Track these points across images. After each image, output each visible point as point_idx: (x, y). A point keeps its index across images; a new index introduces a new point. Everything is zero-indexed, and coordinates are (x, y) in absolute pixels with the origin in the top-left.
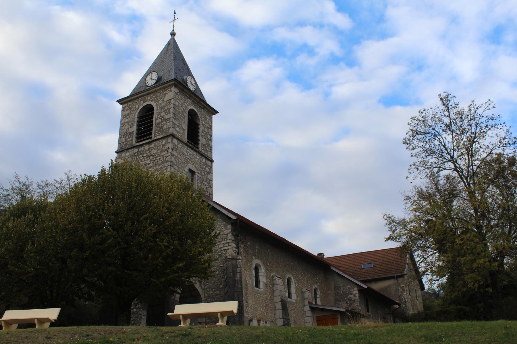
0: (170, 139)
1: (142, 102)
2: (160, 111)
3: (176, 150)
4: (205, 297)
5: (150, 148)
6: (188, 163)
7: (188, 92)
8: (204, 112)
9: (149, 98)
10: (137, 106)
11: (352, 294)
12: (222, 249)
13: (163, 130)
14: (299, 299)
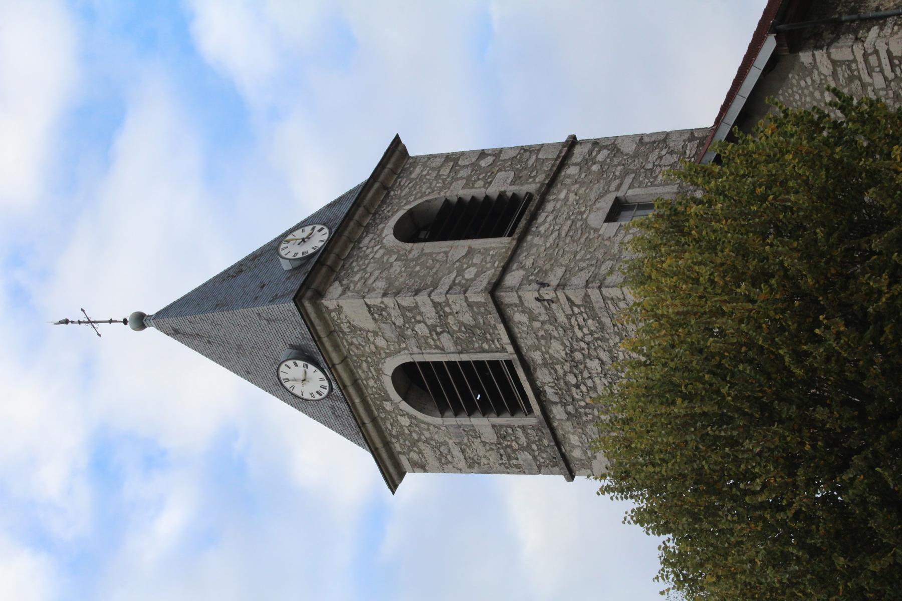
0: (508, 298)
1: (388, 406)
3: (546, 273)
5: (545, 365)
6: (586, 227)
7: (337, 250)
8: (401, 187)
9: (371, 383)
10: (405, 421)
12: (891, 76)
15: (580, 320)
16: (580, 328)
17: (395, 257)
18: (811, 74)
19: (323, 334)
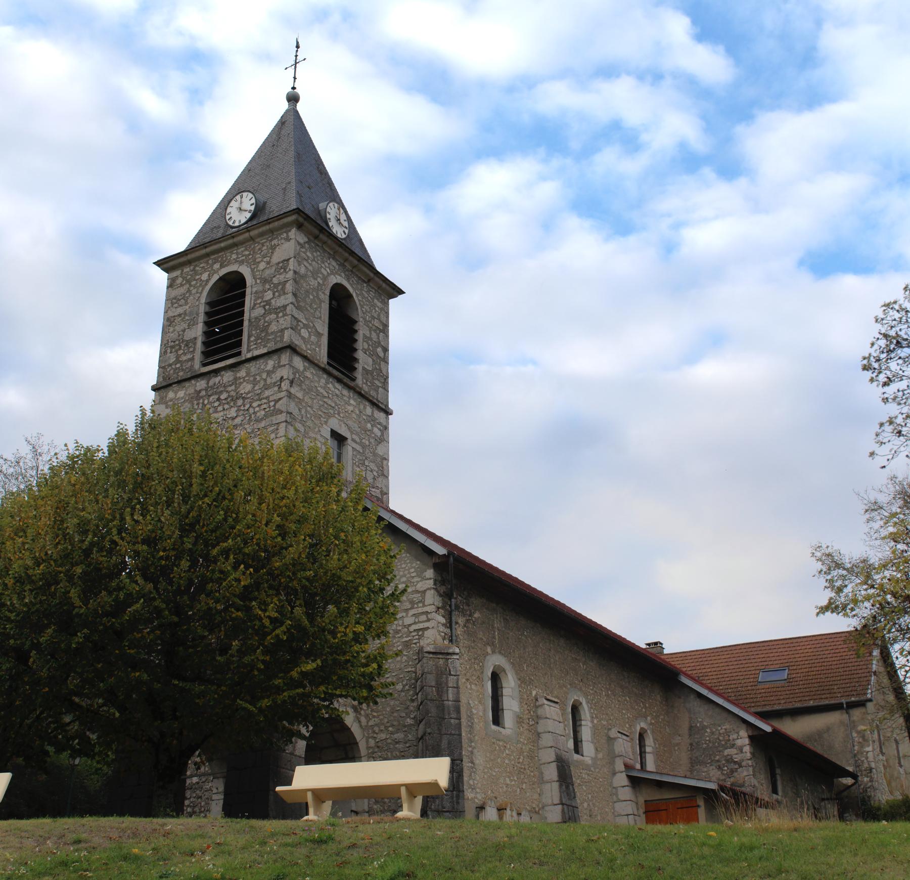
0: (285, 358)
1: (217, 266)
2: (261, 288)
3: (300, 385)
4: (368, 748)
5: (236, 379)
6: (329, 416)
7: (329, 242)
8: (369, 291)
9: (234, 256)
11: (733, 746)
12: (412, 628)
16: (259, 406)
17: (321, 282)
18: (418, 576)
19: (271, 226)
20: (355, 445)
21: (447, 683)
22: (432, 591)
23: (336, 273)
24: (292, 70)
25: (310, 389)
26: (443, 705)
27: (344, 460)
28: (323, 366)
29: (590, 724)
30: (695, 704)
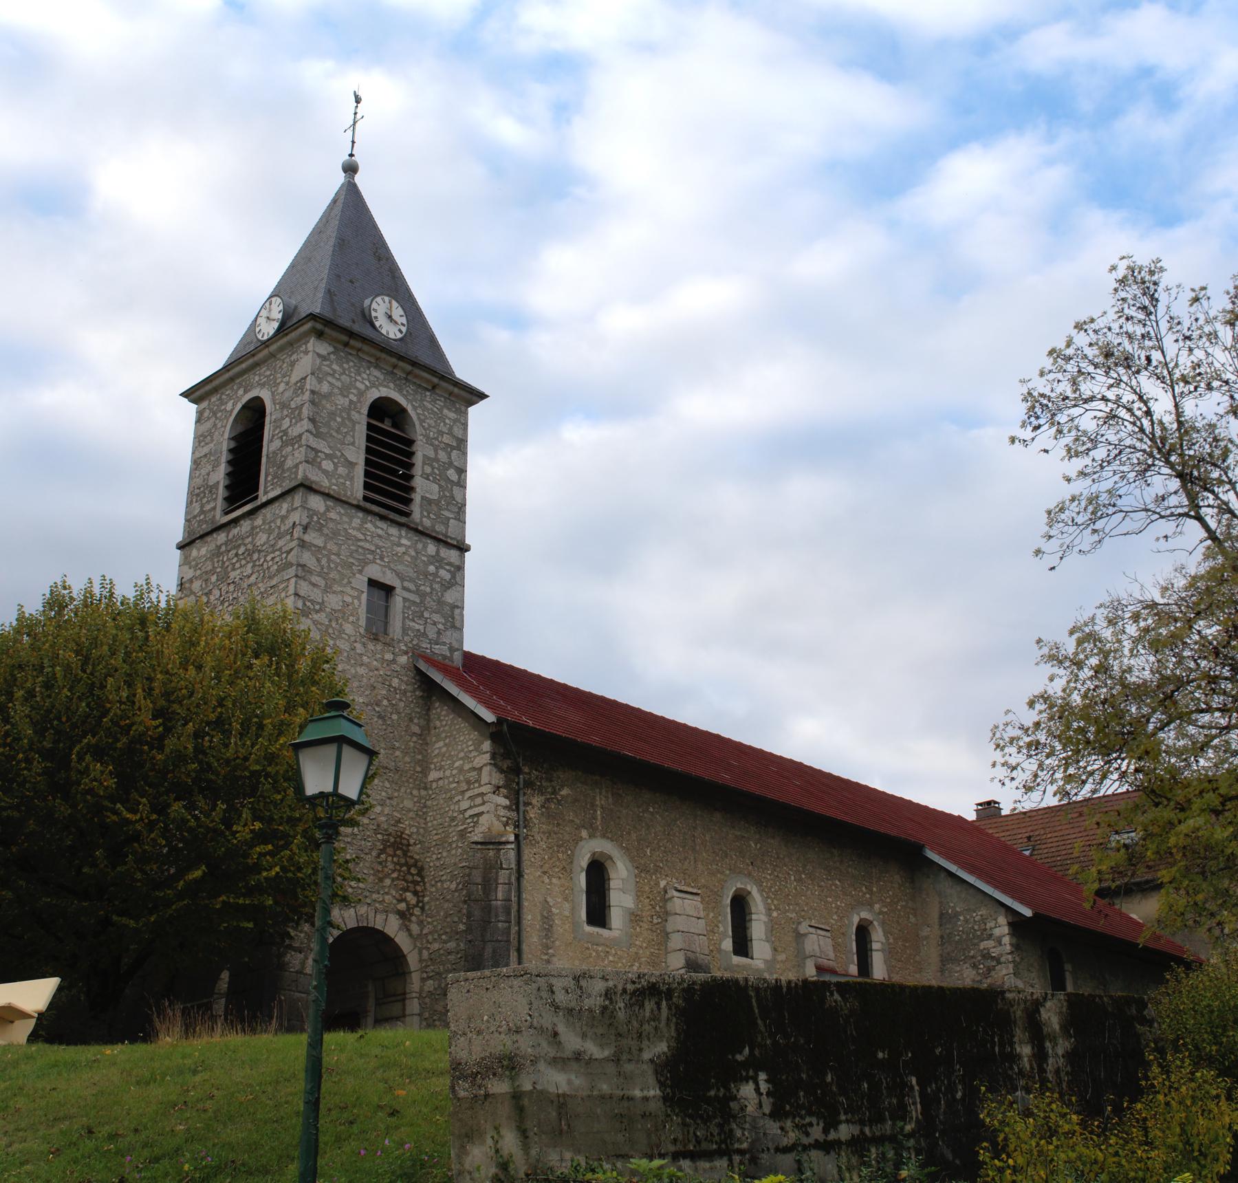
0: (298, 498)
1: (241, 392)
2: (279, 416)
3: (320, 530)
4: (421, 961)
5: (253, 528)
6: (365, 563)
7: (366, 348)
8: (434, 401)
9: (257, 378)
10: (229, 406)
11: (990, 936)
12: (467, 814)
13: (284, 471)
14: (782, 957)
15: (277, 559)
16: (273, 559)
17: (355, 399)
18: (476, 750)
20: (406, 594)
21: (496, 879)
22: (488, 768)
23: (381, 385)
24: (350, 132)
25: (336, 533)
26: (490, 905)
27: (391, 614)
28: (355, 502)
29: (764, 918)
30: (945, 885)
